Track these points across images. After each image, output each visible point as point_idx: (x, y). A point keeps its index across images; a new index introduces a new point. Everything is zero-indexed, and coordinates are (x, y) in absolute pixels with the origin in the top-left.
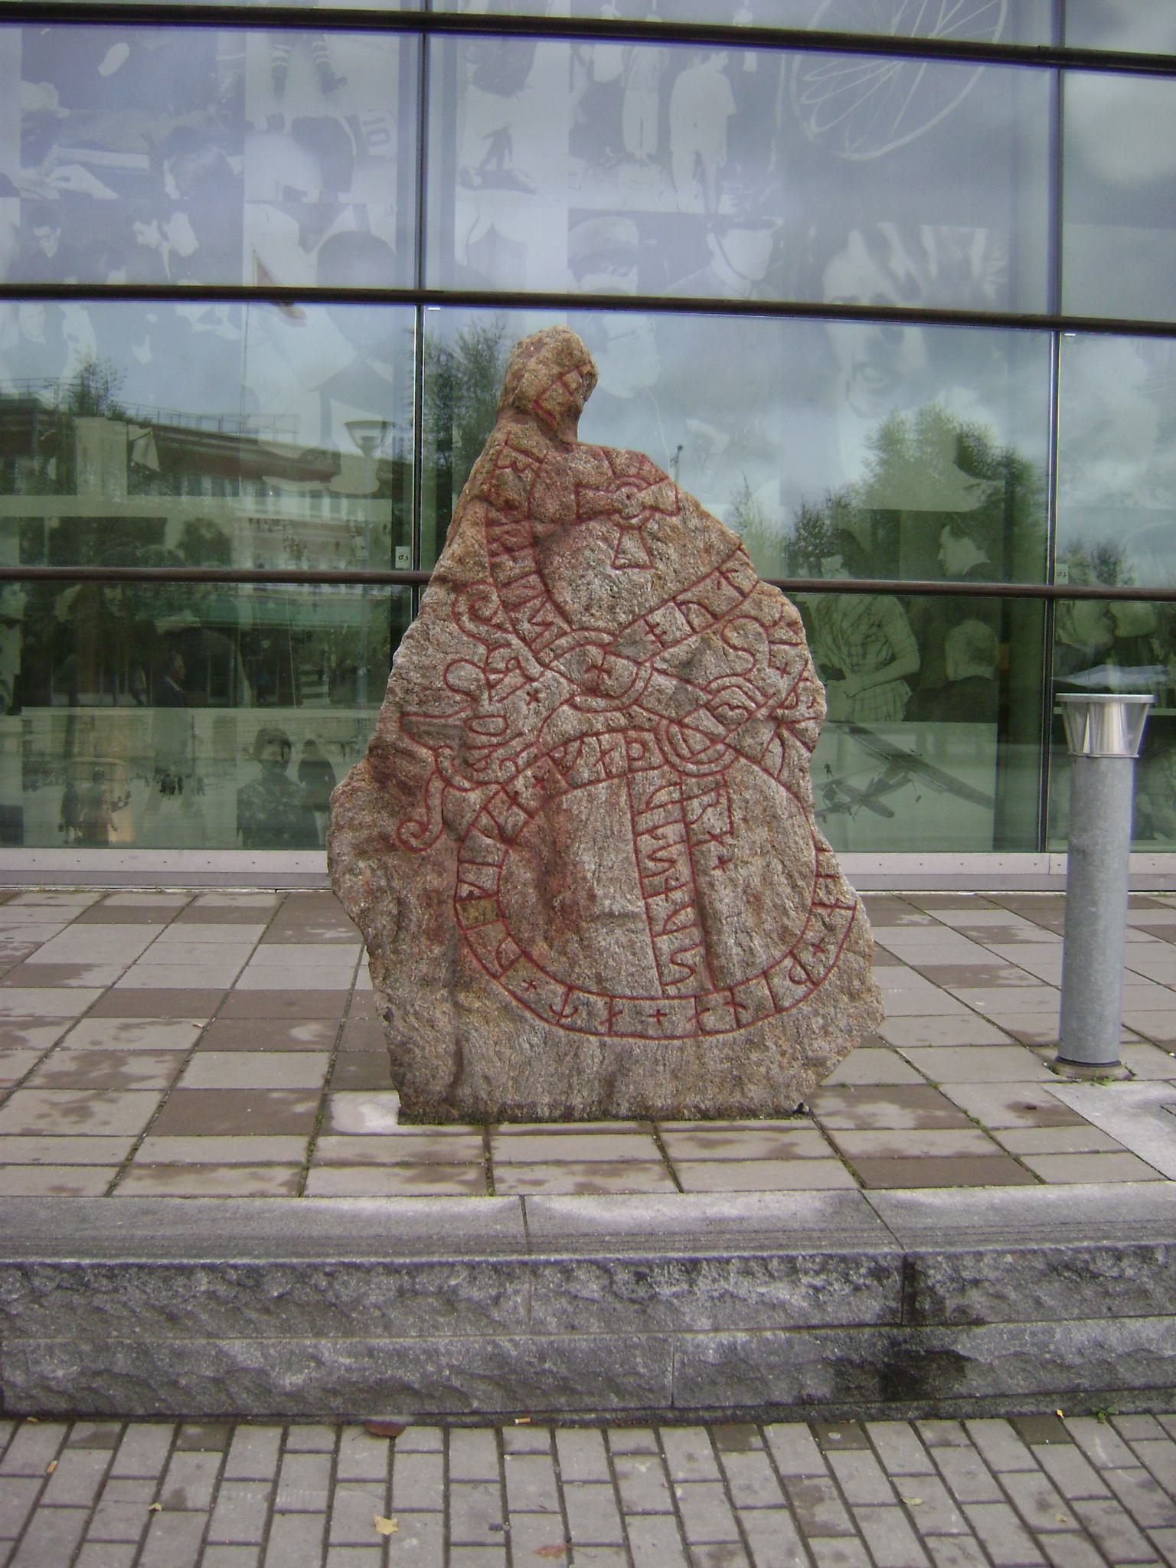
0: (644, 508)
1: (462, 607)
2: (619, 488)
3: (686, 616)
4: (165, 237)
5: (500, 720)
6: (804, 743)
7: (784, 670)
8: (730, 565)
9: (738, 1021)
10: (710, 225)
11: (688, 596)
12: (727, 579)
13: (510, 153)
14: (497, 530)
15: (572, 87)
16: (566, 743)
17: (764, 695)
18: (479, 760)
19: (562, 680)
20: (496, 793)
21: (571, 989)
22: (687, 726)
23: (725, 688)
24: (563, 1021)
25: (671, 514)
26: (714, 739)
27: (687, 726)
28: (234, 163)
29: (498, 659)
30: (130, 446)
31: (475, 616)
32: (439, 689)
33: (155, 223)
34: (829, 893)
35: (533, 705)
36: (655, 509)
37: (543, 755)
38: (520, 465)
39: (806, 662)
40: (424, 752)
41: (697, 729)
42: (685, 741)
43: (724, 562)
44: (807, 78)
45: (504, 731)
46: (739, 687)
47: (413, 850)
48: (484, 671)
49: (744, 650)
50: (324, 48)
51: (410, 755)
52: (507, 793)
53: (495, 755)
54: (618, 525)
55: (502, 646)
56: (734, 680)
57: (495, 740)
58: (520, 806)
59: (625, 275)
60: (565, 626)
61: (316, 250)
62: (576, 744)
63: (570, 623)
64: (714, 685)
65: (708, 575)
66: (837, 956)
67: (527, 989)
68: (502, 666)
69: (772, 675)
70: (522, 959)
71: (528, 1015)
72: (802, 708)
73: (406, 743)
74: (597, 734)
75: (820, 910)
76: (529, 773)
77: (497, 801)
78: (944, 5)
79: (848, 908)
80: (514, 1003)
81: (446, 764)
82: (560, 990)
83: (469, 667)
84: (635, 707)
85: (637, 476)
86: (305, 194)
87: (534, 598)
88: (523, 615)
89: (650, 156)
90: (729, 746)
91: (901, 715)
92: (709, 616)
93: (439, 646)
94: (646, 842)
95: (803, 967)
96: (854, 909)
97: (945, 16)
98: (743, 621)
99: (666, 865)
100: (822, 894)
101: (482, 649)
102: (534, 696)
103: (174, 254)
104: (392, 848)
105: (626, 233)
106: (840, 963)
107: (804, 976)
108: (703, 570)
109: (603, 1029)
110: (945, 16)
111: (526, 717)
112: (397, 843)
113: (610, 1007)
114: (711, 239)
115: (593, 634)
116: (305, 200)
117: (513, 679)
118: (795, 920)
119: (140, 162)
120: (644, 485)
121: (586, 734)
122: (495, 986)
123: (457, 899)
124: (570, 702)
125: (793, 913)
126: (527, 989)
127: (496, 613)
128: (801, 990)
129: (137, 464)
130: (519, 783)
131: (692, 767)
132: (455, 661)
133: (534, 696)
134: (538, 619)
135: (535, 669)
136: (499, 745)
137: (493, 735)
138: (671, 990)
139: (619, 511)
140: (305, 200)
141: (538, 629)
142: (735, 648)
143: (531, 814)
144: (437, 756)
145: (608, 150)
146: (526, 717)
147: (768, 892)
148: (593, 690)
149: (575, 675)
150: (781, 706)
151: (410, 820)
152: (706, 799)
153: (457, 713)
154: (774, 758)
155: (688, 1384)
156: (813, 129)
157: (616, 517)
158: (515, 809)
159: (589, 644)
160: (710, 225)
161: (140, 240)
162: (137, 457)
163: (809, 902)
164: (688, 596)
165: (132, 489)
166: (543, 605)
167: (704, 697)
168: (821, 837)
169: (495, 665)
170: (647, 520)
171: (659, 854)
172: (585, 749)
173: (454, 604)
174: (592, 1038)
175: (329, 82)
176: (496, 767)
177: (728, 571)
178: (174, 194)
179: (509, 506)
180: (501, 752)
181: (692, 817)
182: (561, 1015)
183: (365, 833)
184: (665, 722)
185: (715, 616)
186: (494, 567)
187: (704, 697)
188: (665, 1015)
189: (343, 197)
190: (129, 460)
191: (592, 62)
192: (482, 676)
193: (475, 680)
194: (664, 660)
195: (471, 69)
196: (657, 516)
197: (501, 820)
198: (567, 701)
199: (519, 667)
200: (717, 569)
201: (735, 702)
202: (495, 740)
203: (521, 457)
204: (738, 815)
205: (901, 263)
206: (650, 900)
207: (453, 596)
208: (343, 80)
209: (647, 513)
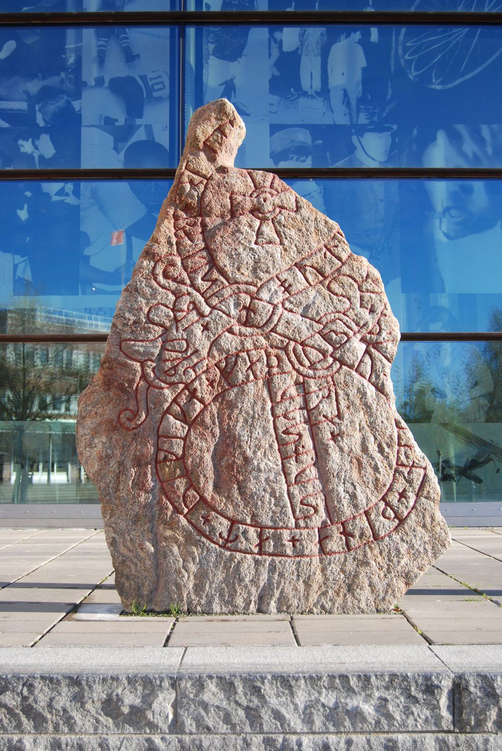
3: (304, 275)
4: (36, 148)
5: (184, 342)
6: (386, 358)
10: (353, 131)
13: (235, 93)
15: (270, 55)
17: (357, 324)
22: (307, 345)
24: (229, 545)
27: (307, 345)
28: (76, 105)
30: (15, 267)
31: (166, 275)
33: (30, 140)
34: (407, 457)
38: (196, 182)
41: (313, 347)
42: (306, 356)
44: (408, 44)
45: (187, 350)
46: (340, 320)
47: (128, 429)
48: (173, 310)
50: (127, 38)
51: (125, 365)
59: (304, 161)
61: (123, 152)
63: (227, 279)
66: (416, 502)
69: (365, 314)
70: (201, 502)
71: (204, 539)
73: (123, 359)
78: (487, 3)
81: (149, 371)
82: (226, 523)
84: (273, 334)
86: (117, 120)
89: (316, 93)
91: (484, 418)
95: (392, 509)
96: (425, 469)
97: (489, 5)
100: (403, 458)
101: (172, 297)
102: (206, 328)
103: (41, 157)
105: (304, 137)
107: (393, 515)
109: (256, 550)
110: (489, 5)
113: (260, 536)
114: (354, 139)
116: (117, 124)
119: (23, 106)
120: (276, 193)
124: (230, 331)
129: (19, 277)
135: (207, 310)
136: (185, 359)
140: (117, 124)
142: (336, 294)
144: (142, 366)
145: (292, 90)
147: (365, 456)
148: (247, 323)
156: (413, 74)
160: (353, 131)
161: (22, 150)
162: (19, 273)
165: (16, 292)
174: (249, 556)
175: (130, 57)
178: (41, 124)
181: (312, 406)
183: (98, 419)
188: (298, 540)
189: (138, 121)
190: (15, 275)
191: (281, 41)
192: (171, 314)
195: (211, 47)
203: (195, 176)
204: (343, 404)
205: (469, 147)
208: (138, 56)
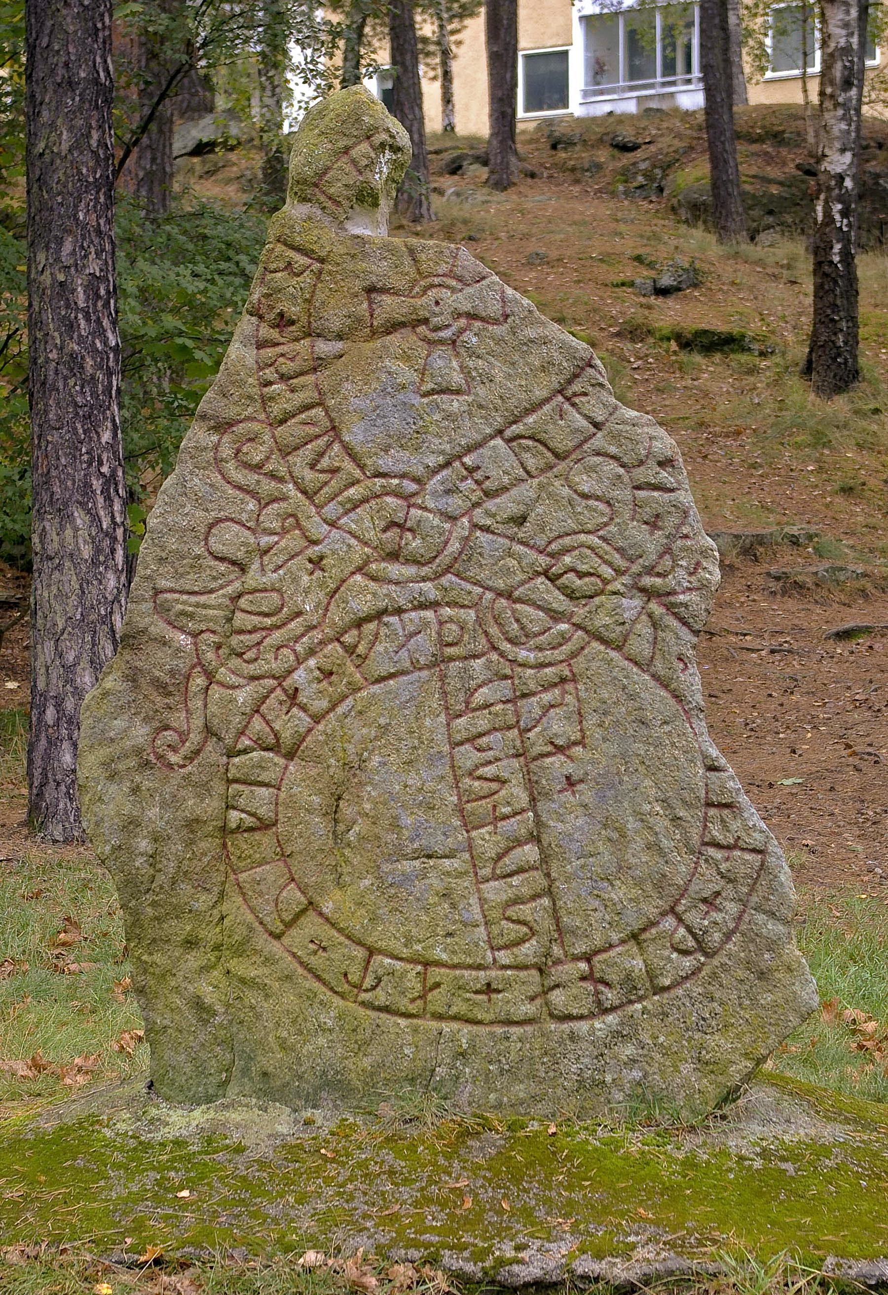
0: (460, 315)
1: (226, 451)
2: (425, 292)
7: (654, 523)
8: (576, 387)
9: (599, 1003)
11: (515, 429)
12: (574, 405)
14: (270, 352)
16: (359, 623)
18: (250, 648)
19: (353, 542)
20: (272, 690)
21: (372, 951)
23: (567, 550)
25: (496, 322)
26: (556, 616)
29: (271, 517)
32: (198, 557)
35: (318, 573)
36: (472, 316)
37: (331, 641)
39: (686, 513)
40: (182, 639)
43: (570, 382)
49: (598, 498)
52: (285, 690)
53: (267, 641)
54: (425, 339)
55: (275, 500)
56: (582, 537)
57: (268, 621)
58: (303, 708)
60: (357, 473)
62: (372, 626)
63: (362, 467)
64: (554, 547)
65: (547, 400)
67: (315, 953)
68: (276, 525)
69: (638, 532)
72: (681, 573)
74: (399, 611)
75: (711, 851)
76: (312, 662)
77: (271, 701)
79: (754, 851)
80: (300, 970)
82: (360, 953)
83: (236, 528)
85: (450, 274)
87: (317, 437)
88: (299, 461)
90: (578, 626)
92: (549, 454)
93: (199, 502)
94: (468, 756)
98: (598, 459)
99: (494, 786)
104: (146, 764)
106: (743, 927)
108: (540, 393)
111: (307, 592)
112: (152, 758)
115: (395, 481)
117: (292, 541)
118: (680, 867)
121: (385, 612)
122: (275, 947)
123: (224, 830)
125: (674, 856)
126: (315, 953)
127: (268, 458)
128: (688, 963)
130: (299, 677)
131: (523, 654)
132: (219, 521)
133: (317, 562)
134: (325, 463)
137: (267, 615)
138: (504, 957)
139: (426, 321)
141: (323, 477)
143: (317, 719)
146: (307, 592)
149: (371, 535)
150: (650, 571)
151: (167, 728)
152: (547, 697)
153: (222, 587)
154: (640, 646)
155: (272, 584)
157: (422, 329)
158: (295, 710)
159: (387, 494)
163: (696, 840)
164: (515, 429)
166: (329, 445)
167: (543, 561)
168: (714, 752)
169: (267, 525)
170: (461, 331)
171: (480, 772)
172: (383, 631)
173: (216, 447)
176: (270, 656)
177: (575, 395)
179: (283, 321)
180: (277, 636)
182: (358, 987)
184: (489, 595)
185: (557, 455)
186: (265, 400)
187: (543, 561)
193: (244, 544)
194: (488, 514)
196: (478, 324)
197: (277, 726)
198: (359, 569)
199: (298, 525)
200: (560, 392)
201: (584, 568)
202: (268, 621)
206: (474, 834)
207: (215, 438)
209: (463, 322)
